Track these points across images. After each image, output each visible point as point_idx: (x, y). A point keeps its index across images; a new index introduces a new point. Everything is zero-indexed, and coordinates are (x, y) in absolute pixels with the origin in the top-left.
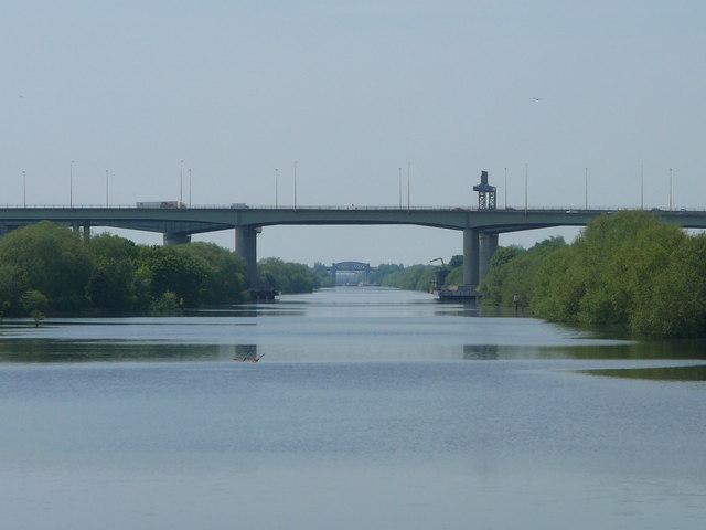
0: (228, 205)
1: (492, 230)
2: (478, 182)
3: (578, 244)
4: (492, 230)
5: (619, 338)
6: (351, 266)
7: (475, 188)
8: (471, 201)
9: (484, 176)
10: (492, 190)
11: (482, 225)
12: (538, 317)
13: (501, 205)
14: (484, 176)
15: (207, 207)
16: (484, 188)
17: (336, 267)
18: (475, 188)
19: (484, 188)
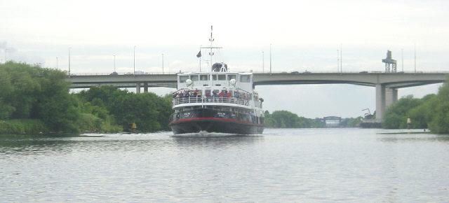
0: (289, 71)
1: (393, 86)
2: (385, 57)
3: (68, 91)
4: (393, 86)
5: (221, 132)
6: (332, 118)
7: (384, 61)
8: (382, 68)
9: (389, 53)
10: (394, 62)
11: (387, 81)
12: (411, 126)
13: (399, 70)
14: (389, 53)
15: (82, 75)
16: (389, 60)
17: (325, 119)
18: (384, 61)
19: (389, 60)
